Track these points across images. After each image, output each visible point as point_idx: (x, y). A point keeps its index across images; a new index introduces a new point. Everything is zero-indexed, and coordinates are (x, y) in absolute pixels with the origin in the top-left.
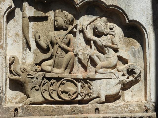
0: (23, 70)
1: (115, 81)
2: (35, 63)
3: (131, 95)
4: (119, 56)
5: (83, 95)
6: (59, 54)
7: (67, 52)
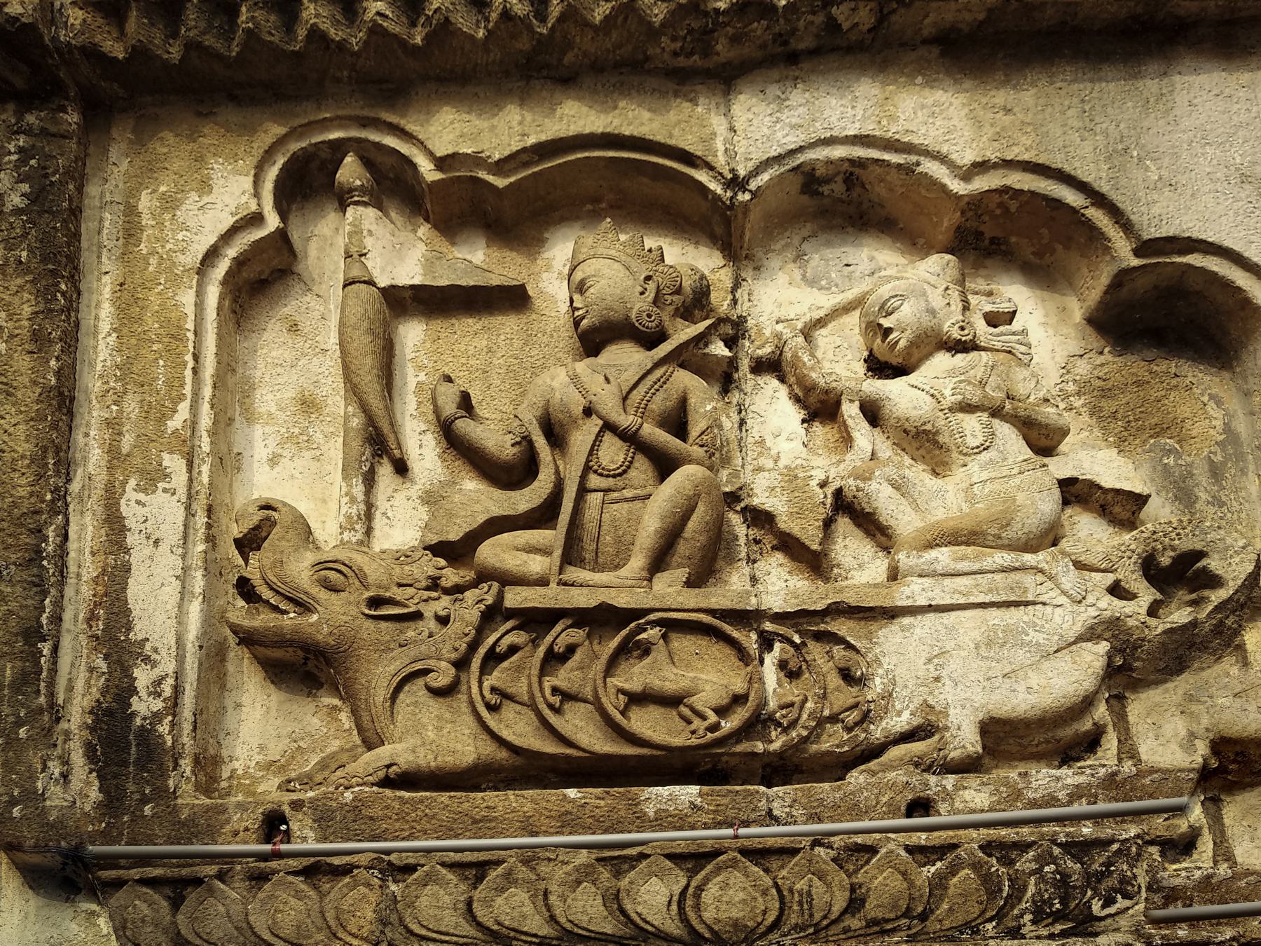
2: (433, 539)
3: (1183, 733)
5: (796, 721)
6: (608, 476)
7: (664, 465)
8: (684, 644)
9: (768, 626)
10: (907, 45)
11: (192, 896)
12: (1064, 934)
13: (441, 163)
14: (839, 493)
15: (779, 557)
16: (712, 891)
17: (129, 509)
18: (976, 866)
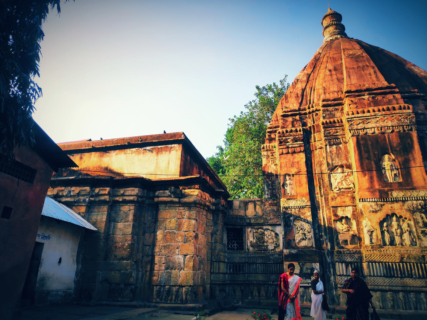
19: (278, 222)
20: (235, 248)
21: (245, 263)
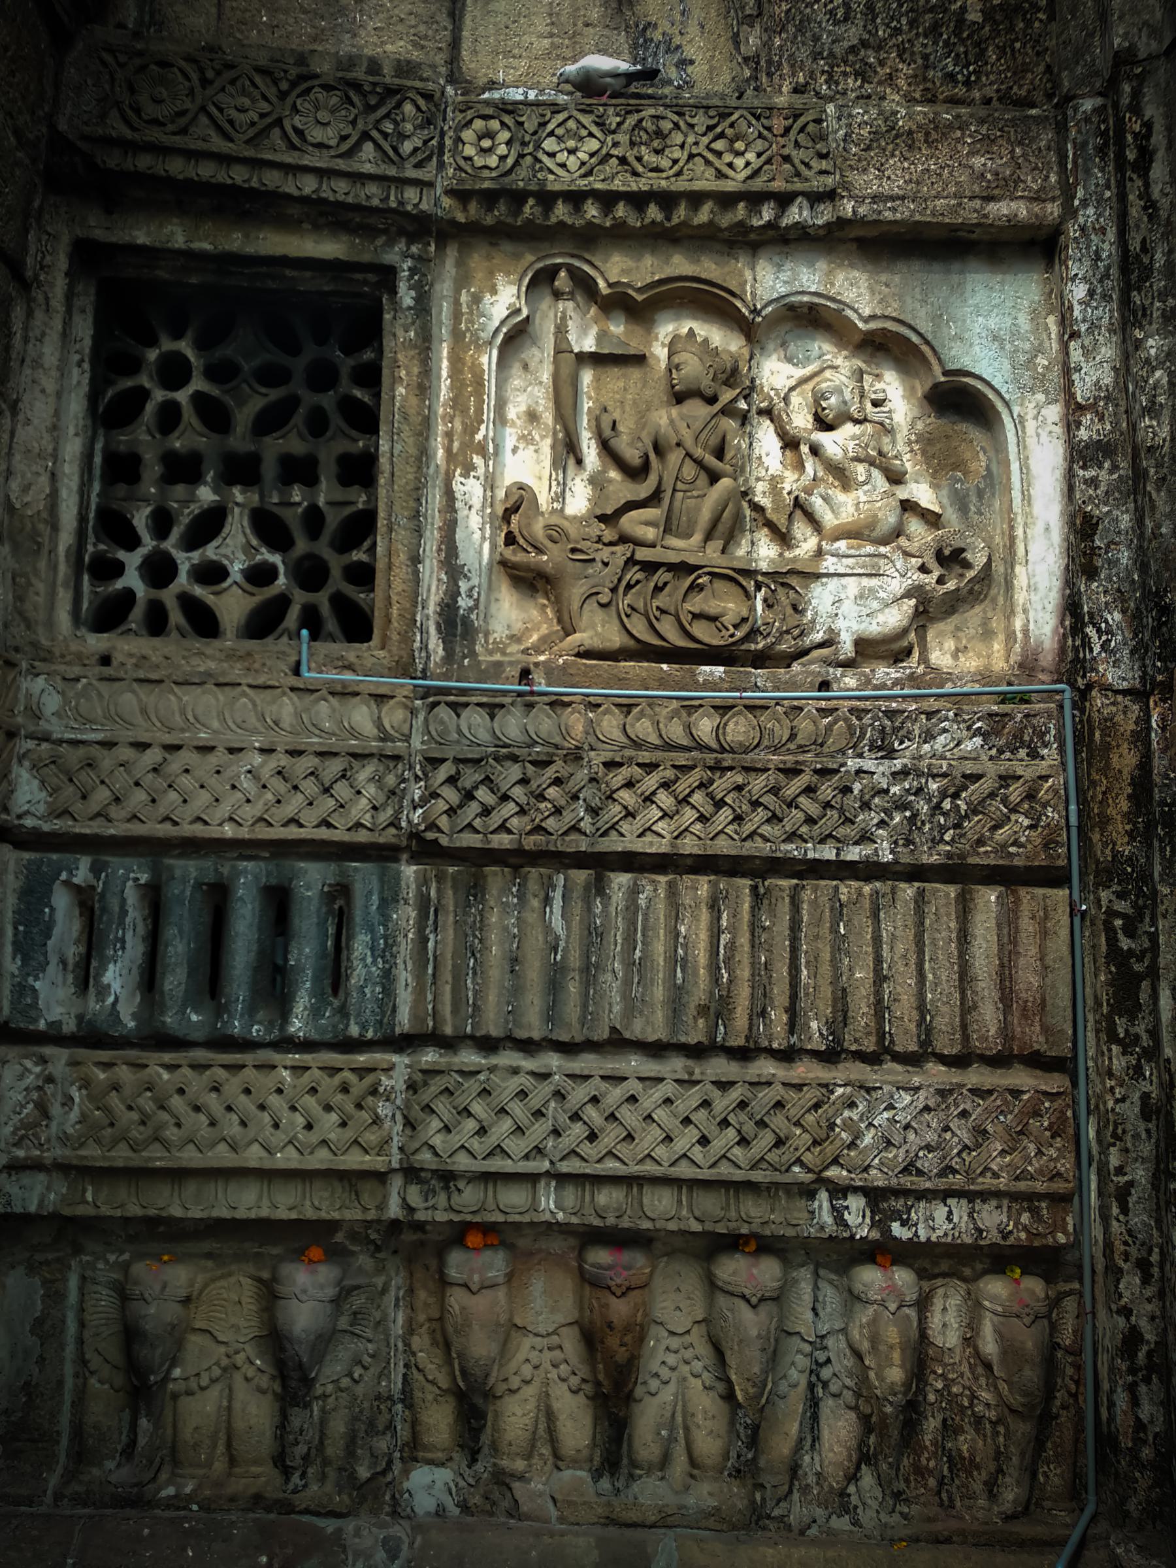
0: (556, 533)
1: (896, 586)
2: (599, 512)
4: (908, 501)
7: (714, 477)
8: (719, 585)
9: (760, 578)
10: (842, 241)
11: (500, 714)
12: (882, 758)
13: (610, 285)
14: (797, 498)
15: (765, 530)
16: (731, 725)
17: (456, 487)
18: (846, 720)
19: (1005, 187)
20: (233, 605)
21: (383, 854)
